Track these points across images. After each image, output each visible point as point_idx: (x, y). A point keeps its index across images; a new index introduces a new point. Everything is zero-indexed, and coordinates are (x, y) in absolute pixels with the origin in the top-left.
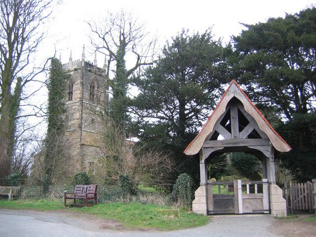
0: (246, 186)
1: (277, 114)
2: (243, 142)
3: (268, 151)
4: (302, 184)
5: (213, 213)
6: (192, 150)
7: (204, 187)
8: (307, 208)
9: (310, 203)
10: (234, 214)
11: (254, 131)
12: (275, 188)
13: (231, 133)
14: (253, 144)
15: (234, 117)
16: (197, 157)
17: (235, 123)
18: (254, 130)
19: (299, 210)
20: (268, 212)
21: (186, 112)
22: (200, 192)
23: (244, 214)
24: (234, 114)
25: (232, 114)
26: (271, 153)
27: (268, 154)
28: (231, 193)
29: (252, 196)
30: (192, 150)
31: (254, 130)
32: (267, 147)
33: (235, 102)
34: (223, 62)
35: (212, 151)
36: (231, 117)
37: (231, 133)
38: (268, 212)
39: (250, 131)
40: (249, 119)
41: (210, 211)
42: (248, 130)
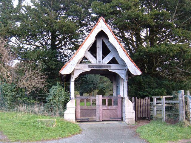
0: (111, 100)
1: (135, 46)
2: (105, 66)
3: (123, 74)
4: (143, 99)
5: (79, 121)
6: (65, 71)
7: (74, 101)
8: (145, 117)
9: (148, 112)
10: (96, 121)
11: (114, 58)
12: (128, 102)
13: (96, 59)
14: (113, 69)
15: (99, 46)
16: (69, 77)
17: (99, 51)
18: (114, 57)
19: (142, 118)
20: (121, 120)
21: (57, 43)
22: (71, 105)
23: (103, 121)
24: (99, 45)
25: (98, 45)
26: (126, 76)
27: (123, 75)
28: (151, 103)
29: (109, 107)
30: (65, 71)
31: (114, 57)
32: (123, 70)
33: (102, 35)
34: (14, 14)
35: (82, 71)
36: (97, 47)
37: (96, 59)
38: (121, 120)
39: (111, 58)
40: (110, 49)
41: (78, 119)
42: (109, 58)
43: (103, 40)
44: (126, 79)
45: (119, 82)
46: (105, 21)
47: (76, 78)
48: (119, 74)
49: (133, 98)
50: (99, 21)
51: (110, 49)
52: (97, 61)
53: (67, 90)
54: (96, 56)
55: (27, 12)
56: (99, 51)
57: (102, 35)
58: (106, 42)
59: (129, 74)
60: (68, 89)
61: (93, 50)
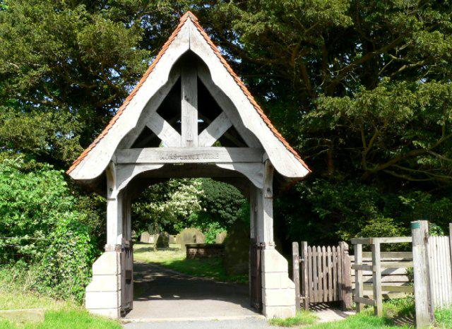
11: (232, 131)
17: (189, 113)
33: (190, 64)
43: (198, 77)
44: (269, 190)
45: (262, 203)
46: (197, 23)
47: (262, 248)
48: (249, 177)
49: (295, 245)
50: (179, 25)
51: (223, 107)
52: (184, 142)
53: (337, 171)
54: (180, 124)
55: (165, 196)
56: (189, 113)
57: (190, 64)
58: (203, 79)
59: (277, 179)
60: (102, 208)
61: (168, 108)
